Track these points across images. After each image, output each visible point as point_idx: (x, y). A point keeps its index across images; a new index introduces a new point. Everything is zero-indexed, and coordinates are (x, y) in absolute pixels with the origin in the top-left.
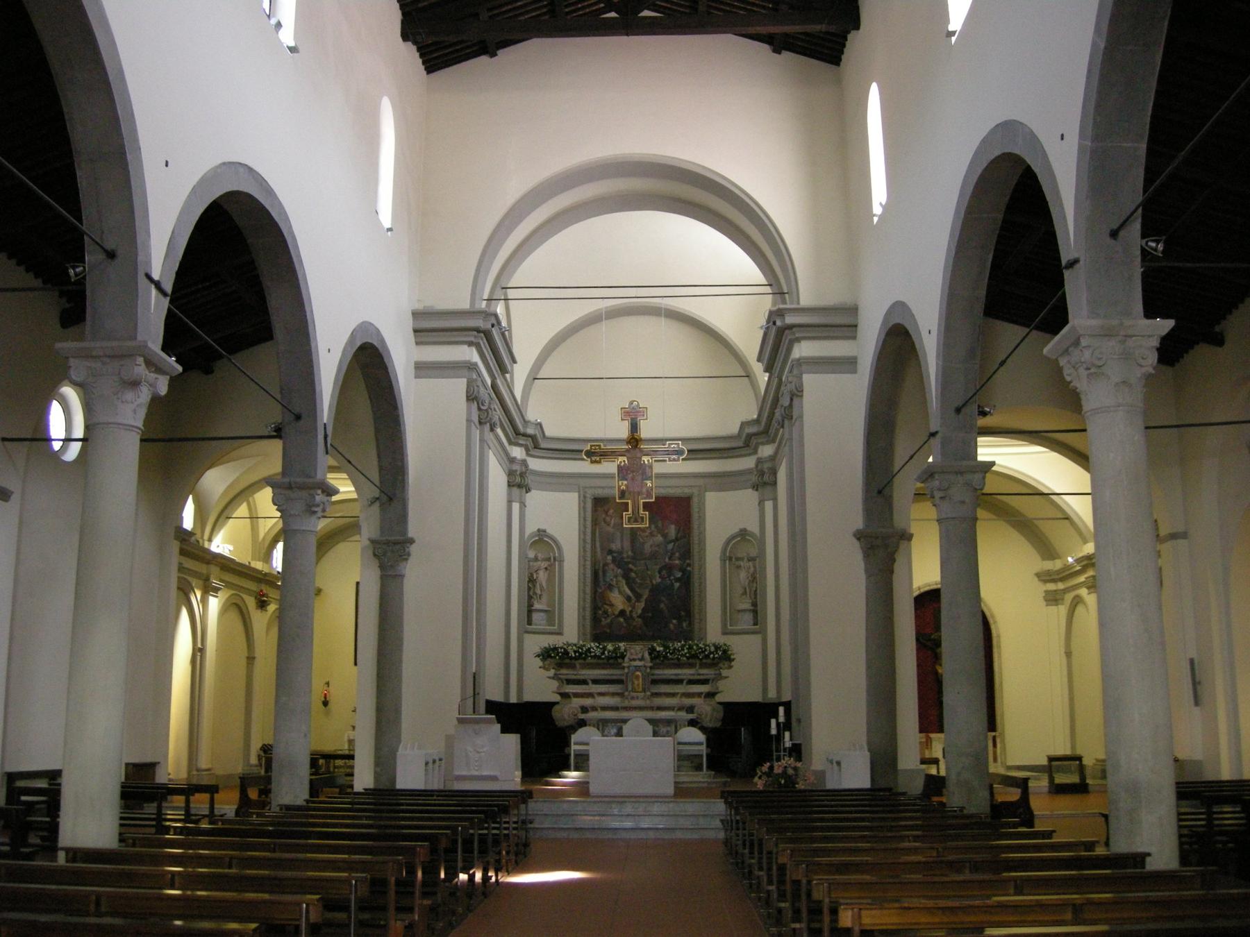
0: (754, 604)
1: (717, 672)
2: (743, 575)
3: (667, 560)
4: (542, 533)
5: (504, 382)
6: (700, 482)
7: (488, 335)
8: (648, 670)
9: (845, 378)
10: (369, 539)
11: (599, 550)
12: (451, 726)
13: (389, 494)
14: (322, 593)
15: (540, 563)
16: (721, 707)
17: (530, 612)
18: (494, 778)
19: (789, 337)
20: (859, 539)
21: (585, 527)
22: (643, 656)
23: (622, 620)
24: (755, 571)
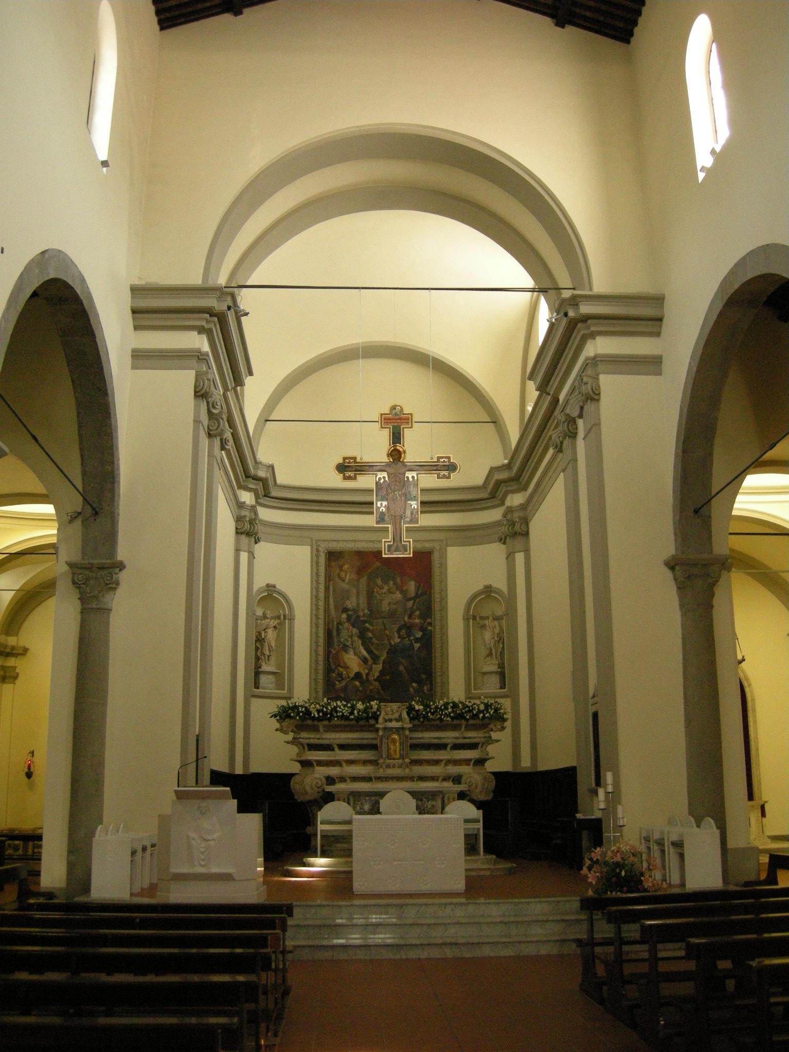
0: (501, 666)
1: (487, 735)
2: (488, 635)
3: (406, 618)
4: (270, 588)
5: (237, 404)
6: (442, 536)
7: (222, 319)
8: (407, 733)
9: (649, 380)
10: (66, 563)
11: (332, 607)
12: (166, 801)
13: (94, 506)
14: (28, 654)
15: (268, 621)
16: (492, 777)
17: (257, 674)
18: (226, 878)
19: (582, 333)
20: (672, 568)
21: (318, 582)
22: (400, 716)
23: (357, 683)
24: (502, 630)
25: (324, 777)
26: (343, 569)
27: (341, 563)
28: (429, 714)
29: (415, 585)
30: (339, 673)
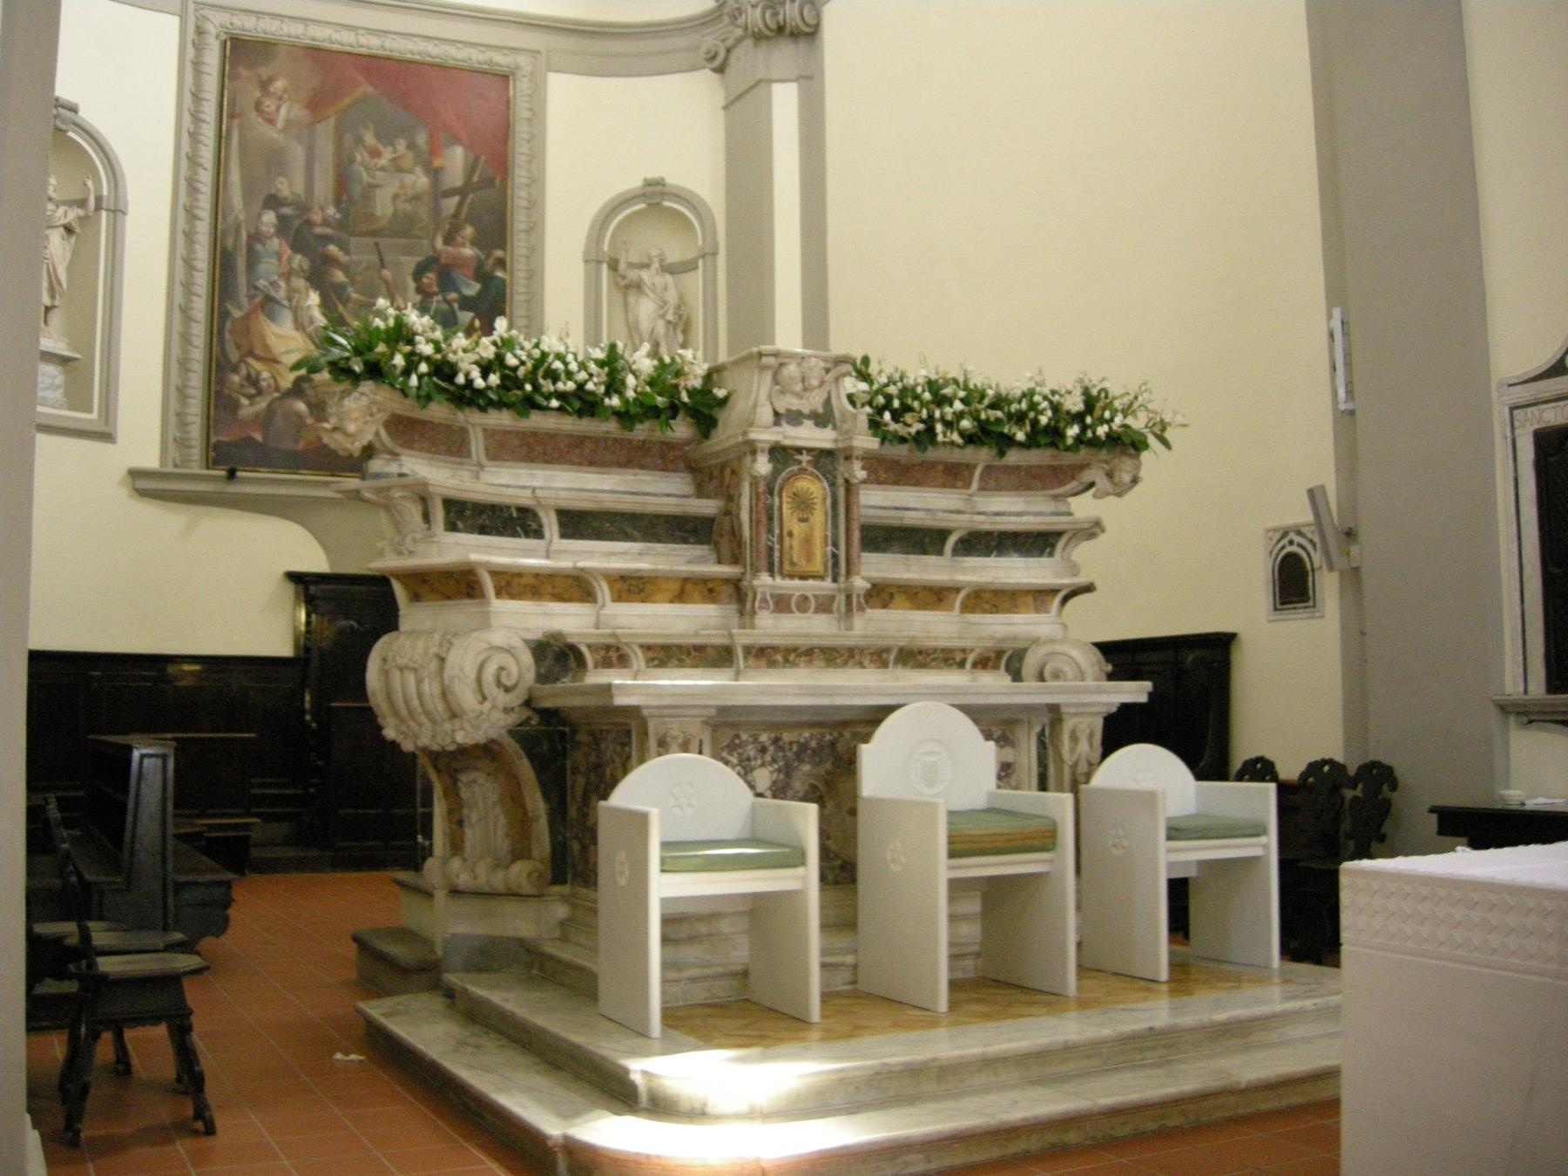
23: (301, 406)
25: (526, 641)
26: (272, 89)
27: (264, 72)
28: (887, 416)
29: (466, 156)
30: (249, 375)
